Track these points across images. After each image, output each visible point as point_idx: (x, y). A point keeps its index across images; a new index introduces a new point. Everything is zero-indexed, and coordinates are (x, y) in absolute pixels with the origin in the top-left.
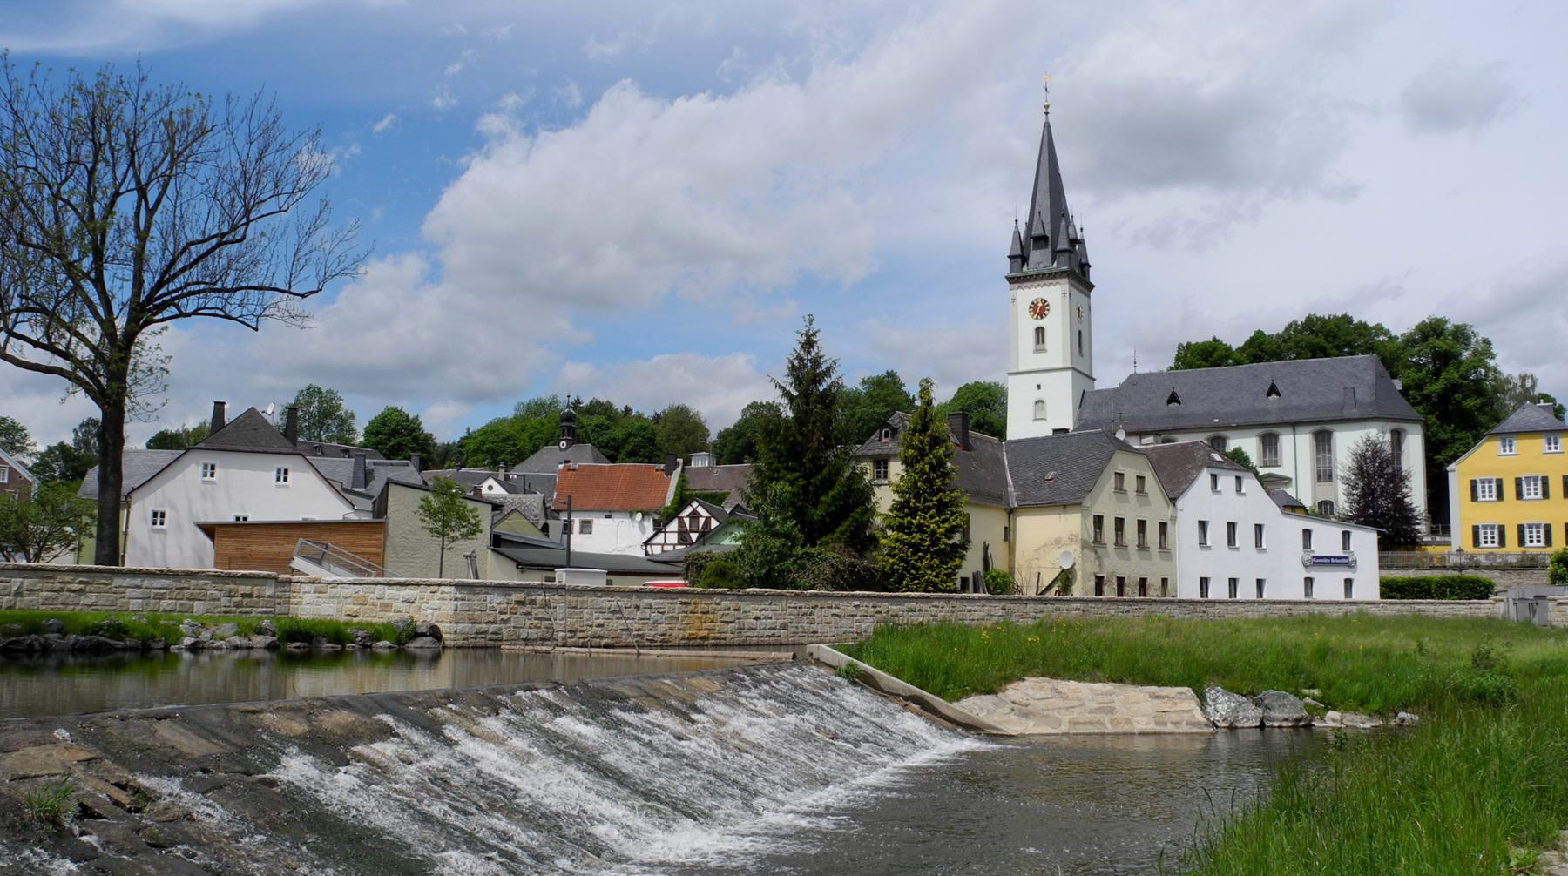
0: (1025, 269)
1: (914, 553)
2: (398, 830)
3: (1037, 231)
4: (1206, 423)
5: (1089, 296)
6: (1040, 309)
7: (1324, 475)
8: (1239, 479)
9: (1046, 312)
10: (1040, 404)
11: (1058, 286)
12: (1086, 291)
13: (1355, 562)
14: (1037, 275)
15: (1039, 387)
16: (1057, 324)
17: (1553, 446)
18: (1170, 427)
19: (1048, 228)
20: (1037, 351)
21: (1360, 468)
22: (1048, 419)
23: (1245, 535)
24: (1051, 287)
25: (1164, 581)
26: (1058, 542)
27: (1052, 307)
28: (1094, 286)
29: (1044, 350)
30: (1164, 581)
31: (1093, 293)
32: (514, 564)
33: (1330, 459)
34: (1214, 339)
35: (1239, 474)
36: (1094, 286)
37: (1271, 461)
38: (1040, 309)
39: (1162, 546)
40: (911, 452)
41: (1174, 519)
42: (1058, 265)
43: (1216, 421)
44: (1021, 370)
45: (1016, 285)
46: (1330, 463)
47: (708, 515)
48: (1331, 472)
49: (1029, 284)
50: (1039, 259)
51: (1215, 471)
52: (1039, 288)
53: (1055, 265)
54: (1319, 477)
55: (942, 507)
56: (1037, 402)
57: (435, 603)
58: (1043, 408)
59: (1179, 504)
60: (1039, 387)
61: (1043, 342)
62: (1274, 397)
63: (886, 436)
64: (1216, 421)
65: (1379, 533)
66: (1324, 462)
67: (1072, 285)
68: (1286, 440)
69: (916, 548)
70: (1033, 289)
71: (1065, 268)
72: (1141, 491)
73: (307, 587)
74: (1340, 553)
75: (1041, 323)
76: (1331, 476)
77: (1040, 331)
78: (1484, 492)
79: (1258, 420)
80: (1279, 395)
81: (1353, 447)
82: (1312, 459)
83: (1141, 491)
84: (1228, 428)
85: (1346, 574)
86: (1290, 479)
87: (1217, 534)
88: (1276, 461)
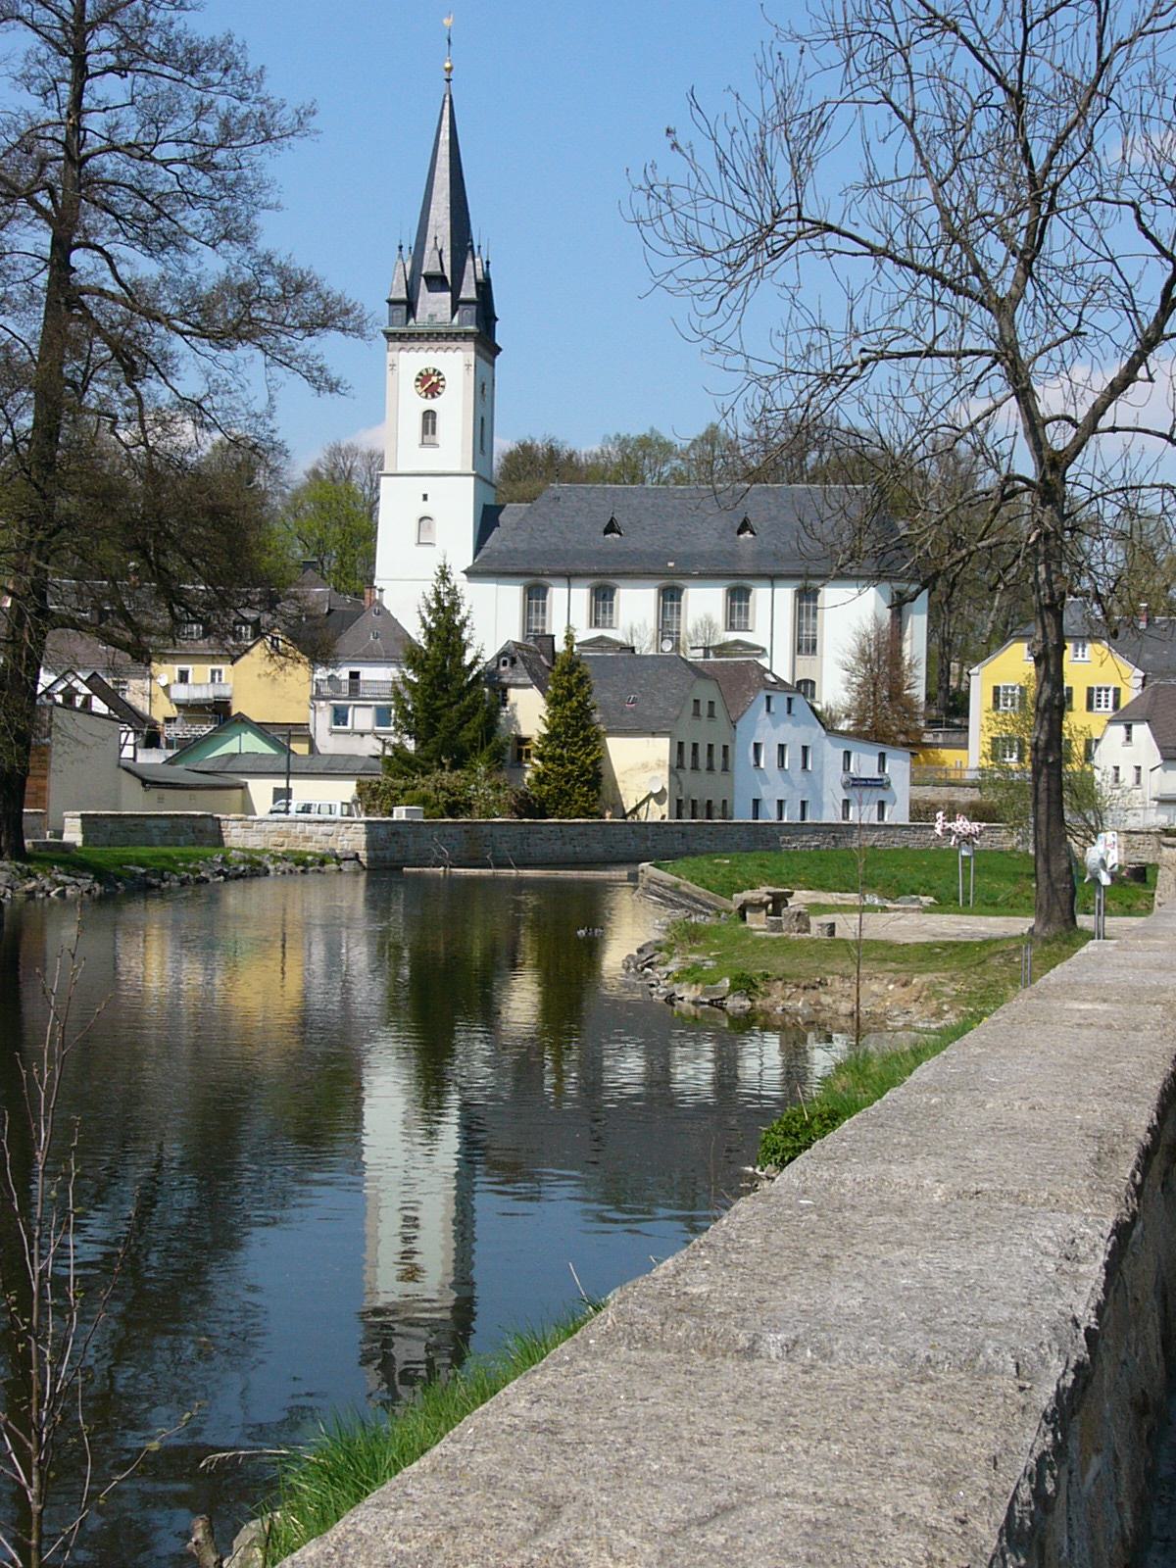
0: (412, 322)
1: (567, 782)
3: (430, 266)
4: (658, 568)
5: (493, 364)
6: (430, 383)
7: (806, 645)
8: (882, 756)
9: (440, 390)
10: (426, 522)
11: (459, 353)
12: (487, 354)
13: (889, 784)
14: (430, 334)
15: (425, 497)
16: (456, 407)
17: (1080, 653)
18: (611, 569)
19: (447, 262)
21: (863, 651)
23: (792, 757)
24: (450, 353)
25: (725, 802)
26: (645, 766)
28: (500, 349)
29: (435, 445)
30: (725, 802)
31: (498, 359)
32: (139, 782)
33: (815, 624)
34: (652, 430)
36: (500, 349)
38: (430, 383)
39: (725, 769)
40: (560, 692)
41: (733, 741)
42: (461, 323)
43: (671, 564)
44: (400, 470)
45: (398, 344)
46: (815, 630)
47: (89, 692)
49: (417, 345)
50: (434, 306)
51: (769, 693)
52: (431, 353)
55: (587, 741)
56: (422, 519)
57: (349, 835)
58: (429, 528)
60: (425, 497)
61: (434, 433)
62: (748, 535)
63: (505, 663)
64: (671, 564)
68: (761, 595)
69: (568, 777)
70: (422, 353)
71: (472, 328)
72: (711, 715)
73: (234, 824)
74: (877, 776)
76: (814, 647)
77: (429, 417)
79: (724, 568)
80: (752, 532)
81: (856, 624)
83: (711, 715)
84: (688, 576)
85: (881, 795)
86: (764, 650)
88: (746, 624)
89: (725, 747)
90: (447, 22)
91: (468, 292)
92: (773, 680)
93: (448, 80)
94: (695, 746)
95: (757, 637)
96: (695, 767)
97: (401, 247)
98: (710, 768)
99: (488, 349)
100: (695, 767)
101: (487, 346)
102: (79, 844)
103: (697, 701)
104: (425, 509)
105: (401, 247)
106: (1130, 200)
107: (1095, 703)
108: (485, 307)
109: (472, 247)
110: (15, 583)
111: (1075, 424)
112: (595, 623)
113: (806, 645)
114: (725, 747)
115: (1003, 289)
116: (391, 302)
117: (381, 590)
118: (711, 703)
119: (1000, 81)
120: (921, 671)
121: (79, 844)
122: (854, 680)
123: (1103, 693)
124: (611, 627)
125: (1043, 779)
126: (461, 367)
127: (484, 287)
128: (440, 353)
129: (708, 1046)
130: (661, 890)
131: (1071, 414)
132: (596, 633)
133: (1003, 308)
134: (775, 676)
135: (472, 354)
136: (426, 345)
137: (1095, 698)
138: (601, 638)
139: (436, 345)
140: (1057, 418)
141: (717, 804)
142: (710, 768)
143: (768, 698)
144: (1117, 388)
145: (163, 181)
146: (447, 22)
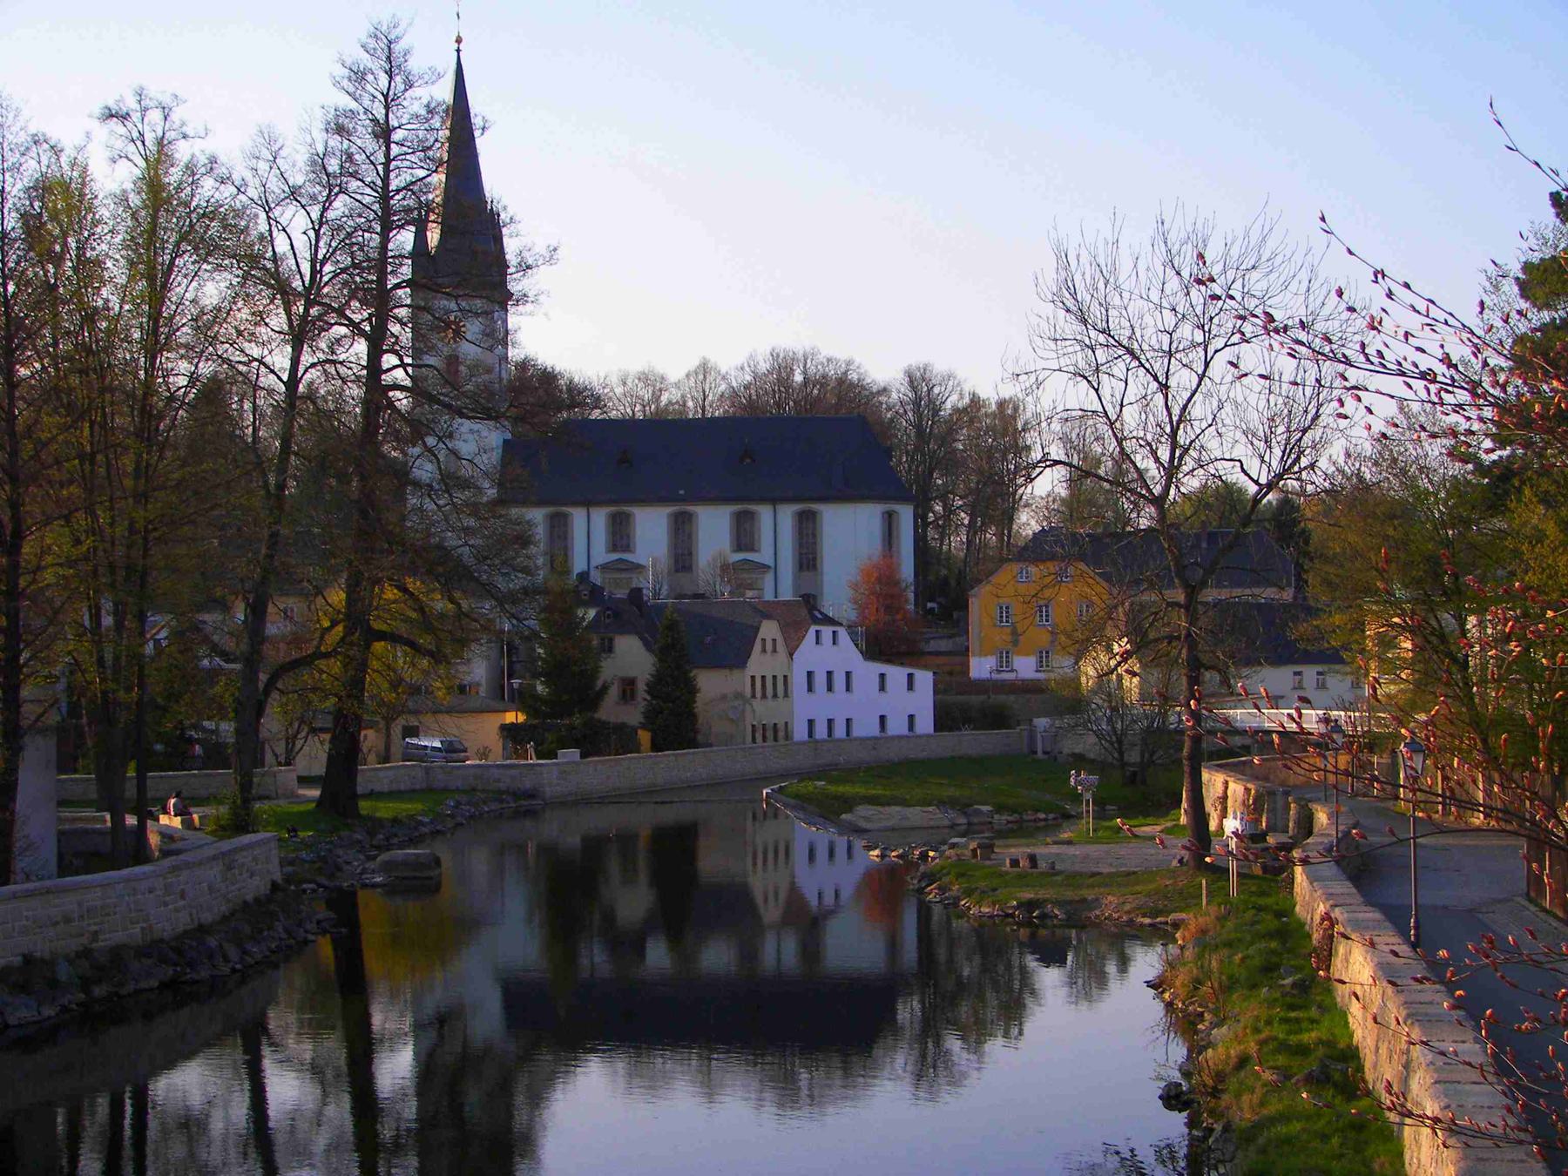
39: (786, 695)
72: (775, 651)
83: (775, 651)
89: (785, 677)
94: (763, 678)
95: (764, 556)
96: (764, 696)
98: (775, 696)
100: (764, 696)
102: (596, 716)
103: (764, 640)
114: (785, 677)
115: (1157, 490)
118: (774, 640)
119: (1156, 378)
121: (596, 716)
122: (638, 408)
125: (1436, 626)
129: (239, 1041)
132: (615, 556)
134: (821, 613)
138: (620, 560)
141: (781, 726)
142: (775, 696)
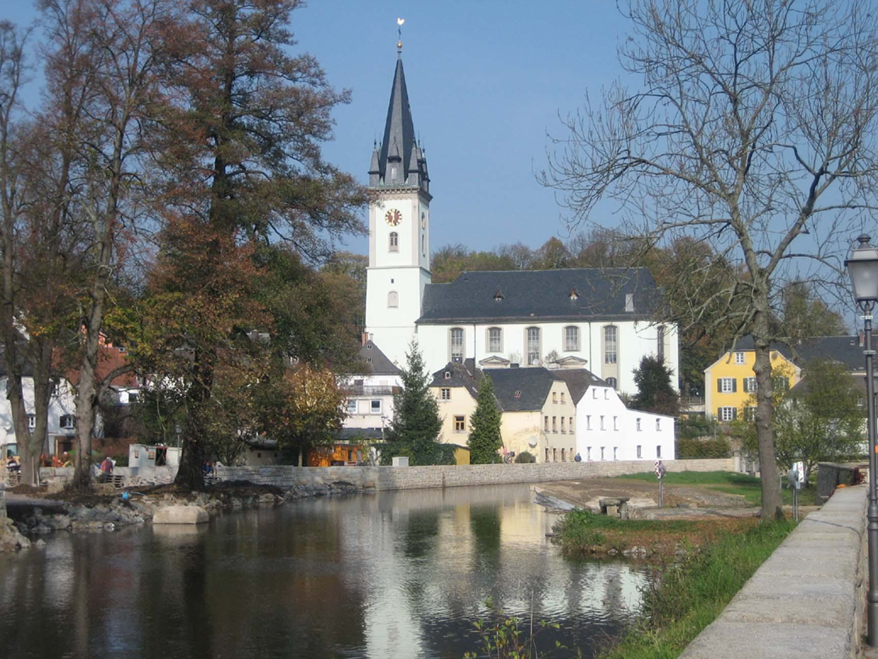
2: (725, 528)
9: (399, 221)
12: (425, 201)
15: (392, 281)
20: (391, 251)
22: (399, 306)
23: (608, 421)
24: (404, 201)
26: (527, 430)
27: (403, 217)
28: (432, 197)
29: (396, 251)
33: (615, 346)
35: (606, 388)
36: (432, 197)
37: (572, 347)
41: (575, 415)
46: (615, 349)
48: (615, 356)
52: (393, 201)
53: (407, 182)
54: (607, 360)
59: (578, 405)
60: (392, 281)
61: (396, 244)
65: (675, 419)
66: (611, 346)
67: (420, 200)
75: (394, 229)
76: (615, 359)
78: (725, 415)
82: (602, 347)
86: (586, 361)
87: (595, 420)
90: (401, 22)
91: (414, 165)
92: (596, 380)
93: (400, 52)
97: (375, 144)
99: (425, 198)
101: (425, 197)
103: (554, 393)
104: (393, 287)
105: (375, 144)
106: (792, 144)
107: (723, 388)
108: (424, 176)
109: (415, 142)
110: (78, 329)
111: (770, 254)
112: (492, 350)
113: (611, 358)
116: (370, 173)
117: (372, 334)
120: (676, 373)
123: (727, 381)
124: (499, 351)
126: (410, 209)
127: (422, 162)
128: (398, 201)
130: (566, 490)
131: (767, 249)
133: (730, 197)
135: (417, 201)
136: (391, 196)
137: (723, 385)
139: (397, 196)
140: (766, 252)
143: (594, 390)
144: (792, 236)
145: (274, 128)
146: (401, 22)
